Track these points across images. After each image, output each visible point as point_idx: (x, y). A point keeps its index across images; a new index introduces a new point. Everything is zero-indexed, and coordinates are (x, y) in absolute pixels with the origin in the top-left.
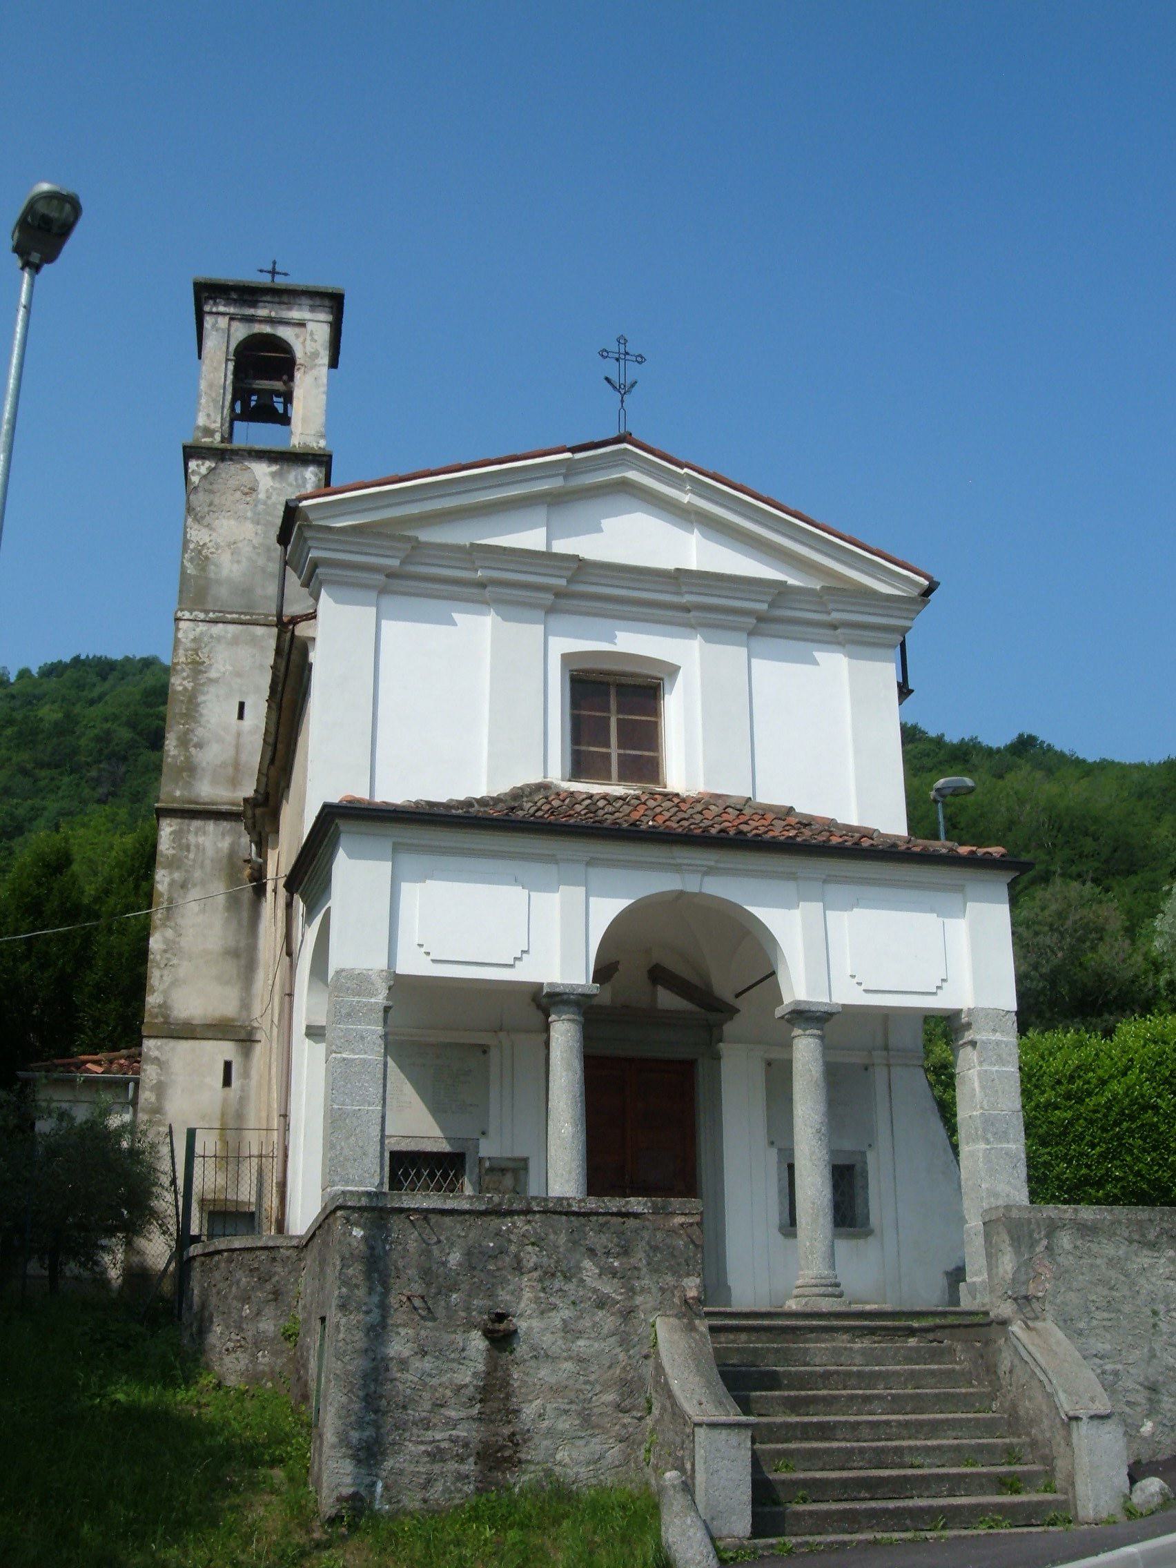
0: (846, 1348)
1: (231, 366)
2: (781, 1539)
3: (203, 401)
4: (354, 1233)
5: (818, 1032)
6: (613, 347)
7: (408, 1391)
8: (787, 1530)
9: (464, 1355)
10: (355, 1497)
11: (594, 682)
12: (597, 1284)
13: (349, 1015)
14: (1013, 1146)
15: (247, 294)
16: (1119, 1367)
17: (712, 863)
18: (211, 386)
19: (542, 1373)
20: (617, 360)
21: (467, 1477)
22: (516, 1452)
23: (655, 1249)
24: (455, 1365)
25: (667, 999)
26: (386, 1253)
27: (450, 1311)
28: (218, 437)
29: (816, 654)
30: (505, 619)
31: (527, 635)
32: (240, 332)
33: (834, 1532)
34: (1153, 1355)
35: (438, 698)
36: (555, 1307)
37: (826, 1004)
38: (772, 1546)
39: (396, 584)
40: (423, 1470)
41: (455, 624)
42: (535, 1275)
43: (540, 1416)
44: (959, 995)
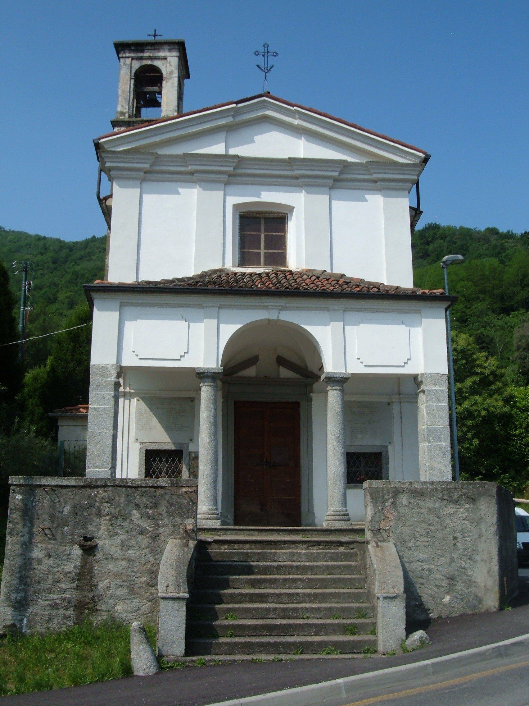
0: (297, 553)
1: (133, 81)
2: (199, 657)
3: (120, 99)
4: (17, 497)
5: (340, 388)
6: (261, 49)
7: (41, 575)
8: (213, 652)
9: (70, 557)
10: (14, 625)
11: (253, 218)
12: (140, 522)
13: (97, 386)
14: (443, 444)
15: (138, 47)
16: (432, 567)
17: (283, 305)
18: (123, 92)
19: (110, 567)
20: (263, 56)
21: (69, 617)
22: (95, 606)
23: (171, 504)
24: (65, 562)
25: (285, 373)
26: (33, 507)
27: (64, 535)
28: (127, 116)
29: (367, 196)
30: (204, 189)
31: (216, 195)
32: (136, 65)
33: (239, 653)
34: (452, 560)
35: (172, 231)
36: (117, 534)
37: (342, 373)
38: (194, 661)
39: (233, 179)
40: (47, 613)
41: (367, 201)
42: (108, 517)
43: (107, 588)
44: (416, 367)
